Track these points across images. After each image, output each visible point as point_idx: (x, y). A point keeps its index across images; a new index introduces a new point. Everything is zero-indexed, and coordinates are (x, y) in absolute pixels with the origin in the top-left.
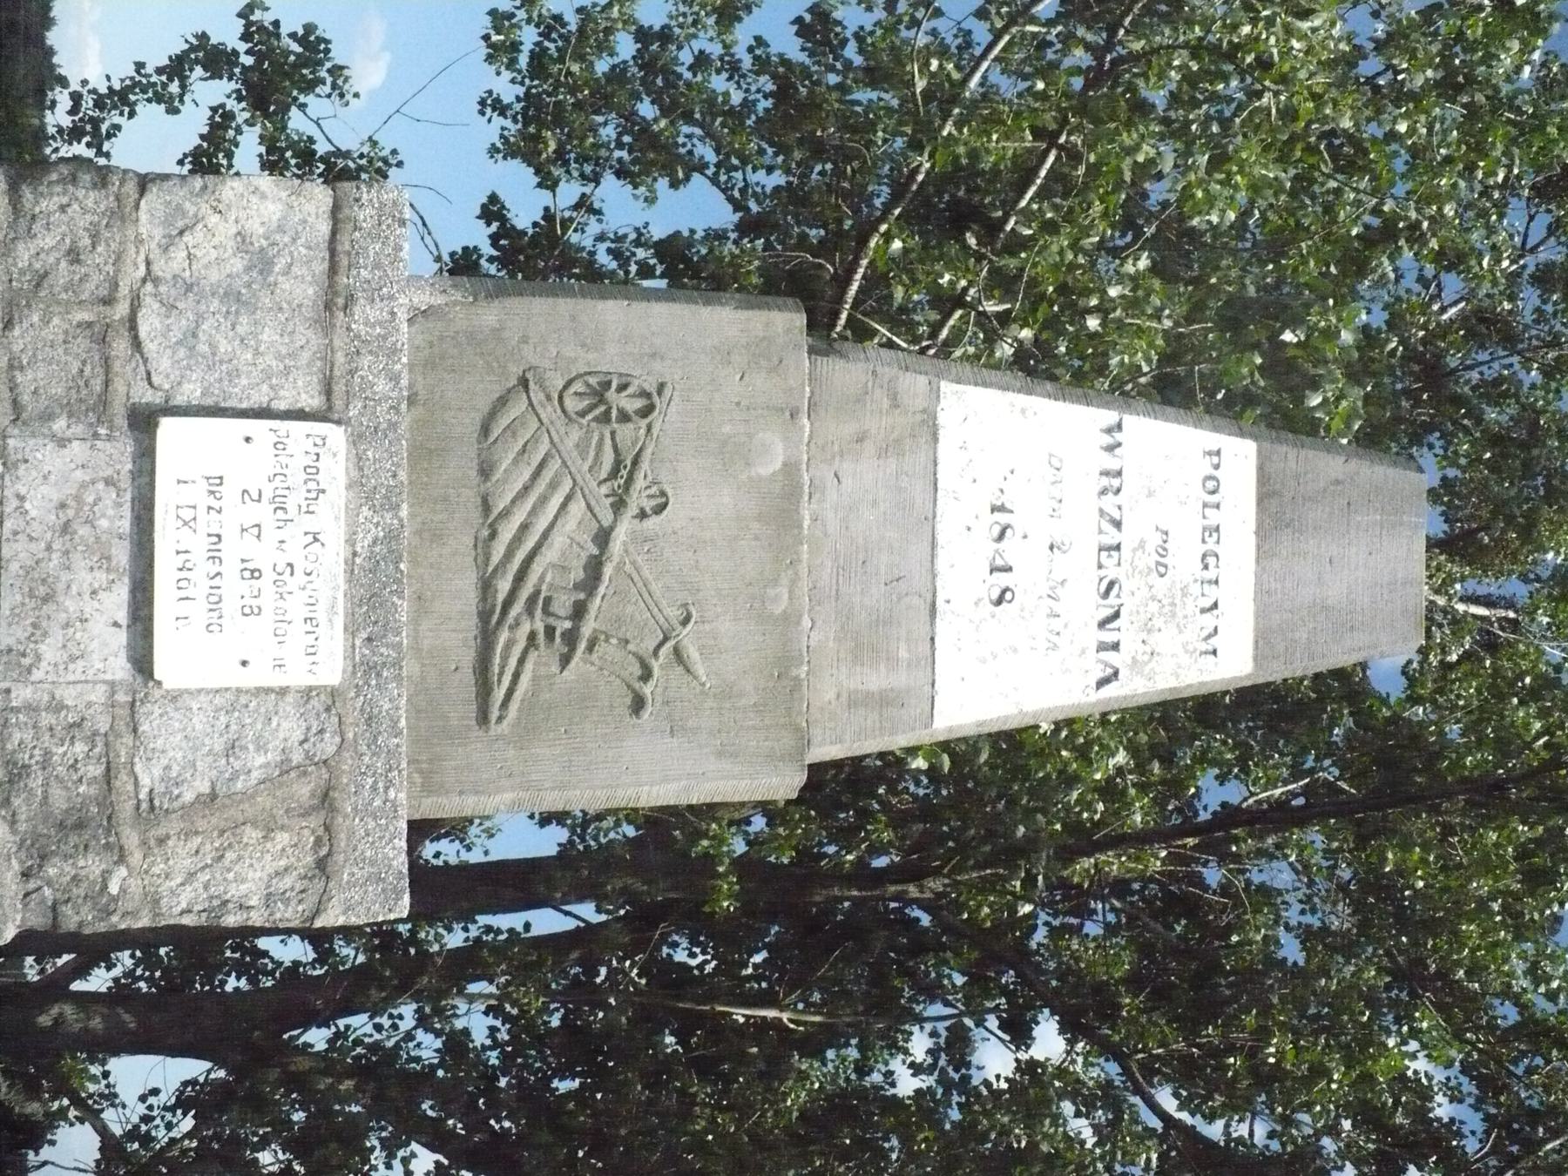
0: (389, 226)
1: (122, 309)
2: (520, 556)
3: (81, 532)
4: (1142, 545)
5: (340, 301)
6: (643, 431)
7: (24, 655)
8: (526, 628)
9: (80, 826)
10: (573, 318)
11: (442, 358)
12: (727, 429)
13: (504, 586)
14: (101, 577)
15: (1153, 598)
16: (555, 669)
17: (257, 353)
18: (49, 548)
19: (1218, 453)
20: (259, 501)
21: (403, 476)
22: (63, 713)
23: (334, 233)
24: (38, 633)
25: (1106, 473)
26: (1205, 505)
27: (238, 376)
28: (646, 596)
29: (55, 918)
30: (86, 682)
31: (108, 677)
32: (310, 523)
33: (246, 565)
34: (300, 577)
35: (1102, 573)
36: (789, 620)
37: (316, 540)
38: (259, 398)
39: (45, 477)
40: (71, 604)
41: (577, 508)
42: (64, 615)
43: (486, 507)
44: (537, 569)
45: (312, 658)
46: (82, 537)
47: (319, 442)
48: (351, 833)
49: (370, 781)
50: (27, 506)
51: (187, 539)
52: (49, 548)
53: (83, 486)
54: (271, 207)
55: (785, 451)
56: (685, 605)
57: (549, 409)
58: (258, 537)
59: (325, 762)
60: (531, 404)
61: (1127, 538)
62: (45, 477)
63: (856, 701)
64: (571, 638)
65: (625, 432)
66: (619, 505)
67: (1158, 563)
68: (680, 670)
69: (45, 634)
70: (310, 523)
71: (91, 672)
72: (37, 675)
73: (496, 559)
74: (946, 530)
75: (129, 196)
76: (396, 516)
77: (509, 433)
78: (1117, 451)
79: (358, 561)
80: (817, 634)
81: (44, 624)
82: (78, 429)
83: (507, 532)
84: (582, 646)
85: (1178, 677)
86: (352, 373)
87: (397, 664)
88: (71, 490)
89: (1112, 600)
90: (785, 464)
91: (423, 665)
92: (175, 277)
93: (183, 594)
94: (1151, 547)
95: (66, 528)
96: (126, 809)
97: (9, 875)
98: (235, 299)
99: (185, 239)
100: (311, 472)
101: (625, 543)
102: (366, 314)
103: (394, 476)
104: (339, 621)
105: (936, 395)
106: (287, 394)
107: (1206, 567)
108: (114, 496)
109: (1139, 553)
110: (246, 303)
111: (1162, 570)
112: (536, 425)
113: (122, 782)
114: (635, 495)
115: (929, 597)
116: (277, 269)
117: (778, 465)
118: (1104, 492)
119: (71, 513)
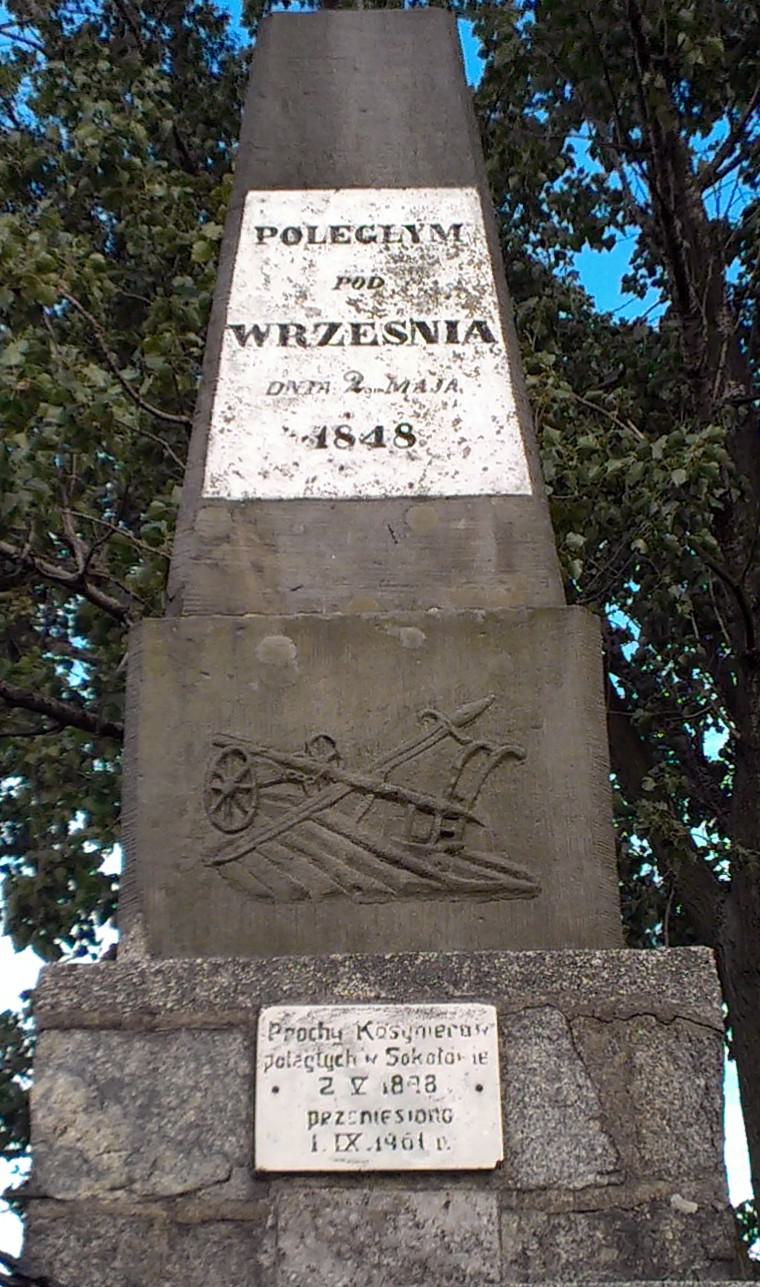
1: (157, 1210)
2: (384, 866)
4: (352, 303)
5: (147, 1018)
6: (259, 760)
9: (633, 1236)
10: (155, 824)
12: (255, 686)
13: (404, 876)
15: (405, 290)
16: (481, 832)
17: (195, 1088)
18: (378, 1266)
19: (260, 230)
20: (331, 1079)
21: (305, 959)
22: (529, 1253)
23: (83, 1027)
25: (284, 341)
26: (312, 241)
27: (217, 1103)
28: (413, 752)
29: (721, 1260)
30: (500, 1231)
31: (495, 1211)
33: (389, 1089)
34: (400, 1042)
35: (380, 340)
36: (430, 626)
37: (365, 1029)
38: (235, 1085)
39: (313, 1270)
40: (430, 1246)
41: (332, 816)
42: (439, 1252)
43: (334, 894)
44: (388, 849)
45: (473, 1030)
47: (276, 1029)
49: (585, 981)
51: (366, 1141)
52: (378, 1266)
55: (273, 633)
56: (420, 720)
57: (241, 842)
59: (568, 1021)
60: (236, 859)
61: (347, 317)
62: (313, 1270)
63: (507, 566)
64: (452, 816)
65: (263, 774)
66: (327, 778)
67: (370, 287)
68: (478, 722)
69: (457, 1268)
73: (379, 884)
74: (345, 488)
76: (342, 963)
78: (263, 329)
79: (383, 995)
80: (445, 603)
81: (446, 1269)
82: (268, 1243)
84: (458, 807)
85: (481, 263)
86: (211, 1005)
87: (478, 960)
89: (407, 331)
90: (286, 633)
93: (417, 1144)
94: (354, 294)
96: (621, 1196)
99: (91, 1157)
100: (304, 1034)
101: (364, 773)
102: (157, 994)
103: (305, 965)
104: (450, 1007)
105: (217, 502)
107: (373, 239)
109: (361, 305)
110: (151, 1099)
111: (377, 281)
112: (254, 854)
113: (592, 1199)
114: (318, 765)
115: (407, 503)
116: (118, 1075)
117: (288, 640)
118: (302, 342)
119: (345, 1247)
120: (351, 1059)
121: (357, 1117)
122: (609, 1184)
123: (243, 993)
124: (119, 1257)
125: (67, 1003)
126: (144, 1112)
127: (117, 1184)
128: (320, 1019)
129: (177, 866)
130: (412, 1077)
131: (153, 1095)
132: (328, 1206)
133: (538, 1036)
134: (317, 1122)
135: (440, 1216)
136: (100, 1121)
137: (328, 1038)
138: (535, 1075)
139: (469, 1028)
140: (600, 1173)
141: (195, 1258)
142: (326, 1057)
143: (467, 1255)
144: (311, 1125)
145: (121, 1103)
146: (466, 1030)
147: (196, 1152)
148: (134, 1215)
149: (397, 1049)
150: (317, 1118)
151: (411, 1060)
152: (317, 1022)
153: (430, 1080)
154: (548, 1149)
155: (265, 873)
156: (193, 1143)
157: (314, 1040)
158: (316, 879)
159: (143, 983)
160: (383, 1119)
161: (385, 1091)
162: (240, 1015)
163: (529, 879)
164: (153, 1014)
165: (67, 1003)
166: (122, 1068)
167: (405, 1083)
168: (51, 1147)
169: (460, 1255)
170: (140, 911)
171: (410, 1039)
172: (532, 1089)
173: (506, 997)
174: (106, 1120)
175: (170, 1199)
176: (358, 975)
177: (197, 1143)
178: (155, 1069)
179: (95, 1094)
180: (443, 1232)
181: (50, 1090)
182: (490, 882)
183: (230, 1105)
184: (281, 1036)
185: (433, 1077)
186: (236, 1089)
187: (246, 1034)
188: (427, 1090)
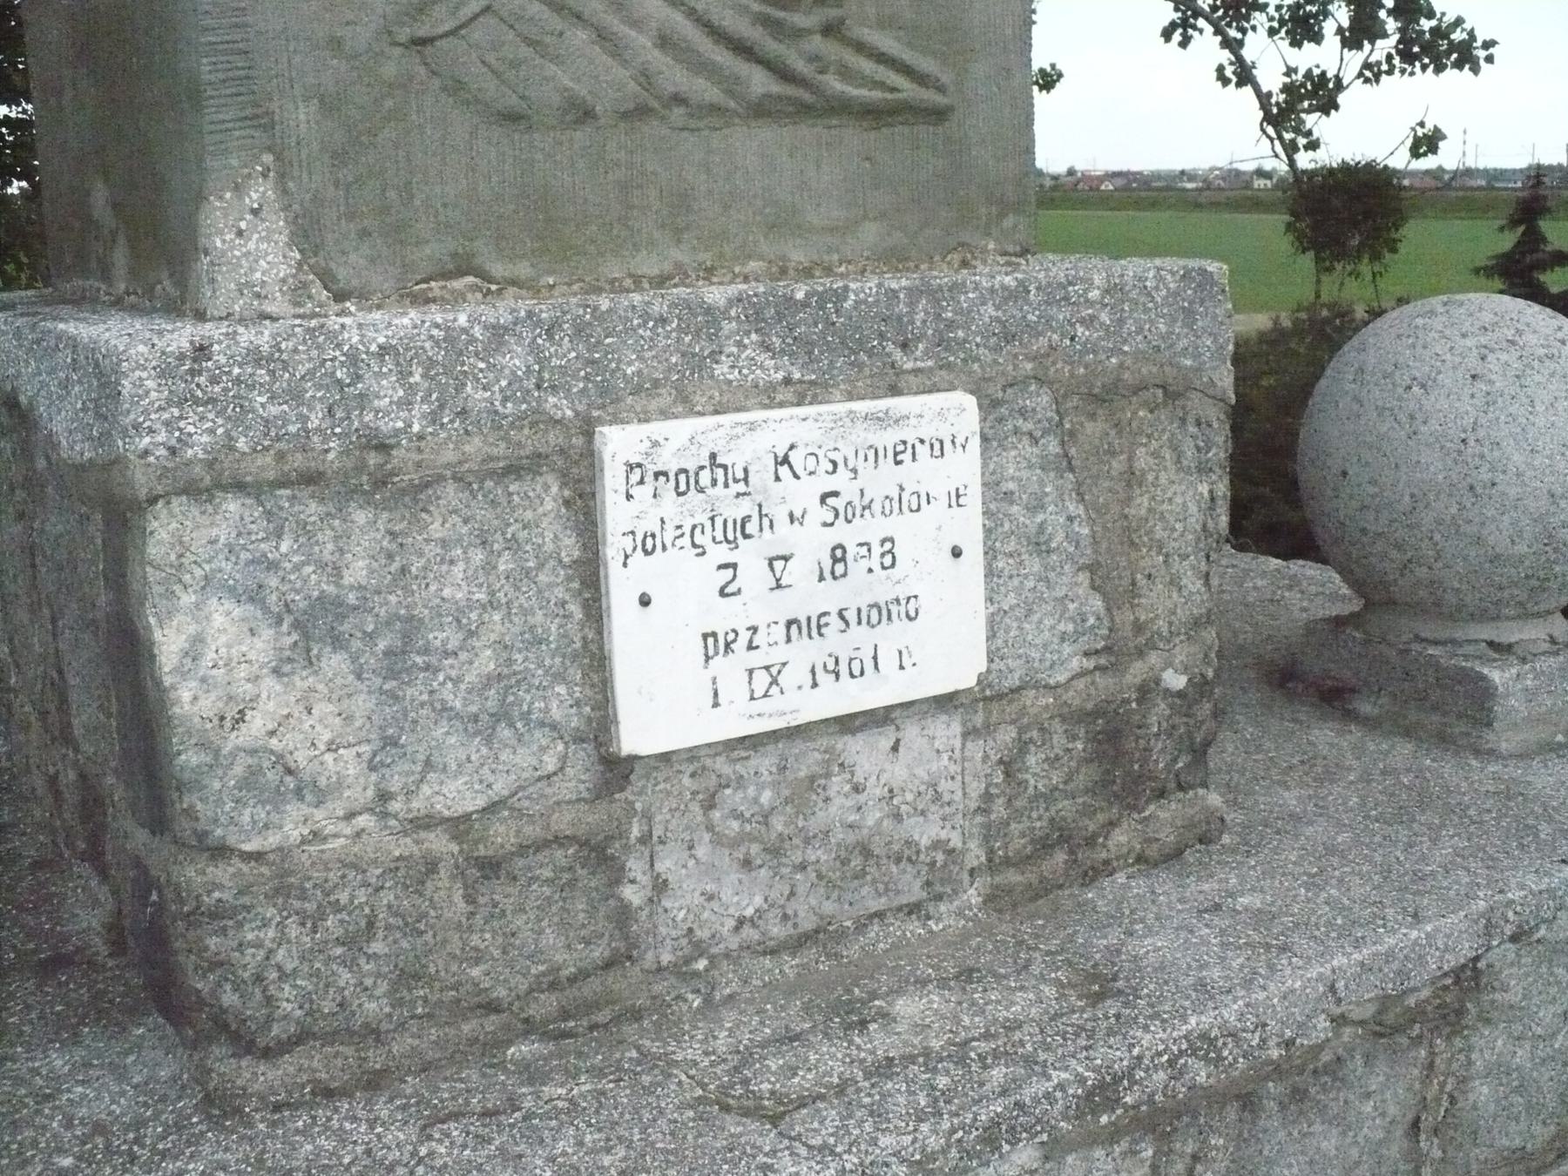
0: (214, 380)
2: (722, 57)
3: (780, 828)
5: (373, 459)
7: (933, 864)
8: (817, 43)
11: (385, 210)
13: (760, 82)
14: (838, 784)
18: (803, 867)
20: (734, 566)
23: (239, 487)
24: (907, 852)
27: (532, 628)
31: (958, 743)
32: (762, 474)
33: (827, 574)
34: (841, 481)
37: (785, 460)
38: (557, 585)
39: (711, 898)
42: (885, 823)
43: (641, 112)
45: (948, 446)
46: (786, 824)
48: (1139, 356)
49: (1080, 330)
50: (749, 912)
51: (794, 676)
52: (803, 867)
53: (718, 840)
54: (218, 620)
58: (786, 559)
60: (453, 32)
62: (711, 898)
70: (762, 474)
71: (954, 768)
72: (956, 841)
73: (705, 90)
75: (239, 873)
77: (510, 75)
79: (797, 376)
81: (896, 847)
82: (636, 866)
83: (675, 77)
88: (724, 859)
91: (865, 217)
92: (372, 768)
95: (775, 851)
97: (1162, 815)
98: (403, 656)
99: (303, 763)
100: (685, 482)
102: (392, 407)
103: (663, 321)
106: (549, 535)
108: (728, 791)
110: (407, 637)
116: (331, 589)
120: (766, 522)
121: (780, 630)
122: (1096, 668)
123: (554, 389)
124: (380, 934)
125: (205, 439)
126: (396, 665)
127: (357, 806)
128: (711, 447)
129: (335, 44)
130: (861, 545)
131: (410, 627)
132: (728, 786)
133: (1016, 431)
134: (717, 653)
135: (888, 766)
136: (312, 690)
137: (726, 485)
138: (1012, 503)
139: (941, 443)
140: (1086, 654)
141: (514, 912)
142: (725, 521)
143: (921, 819)
144: (708, 658)
145: (346, 648)
146: (937, 446)
147: (504, 732)
148: (398, 859)
149: (835, 494)
150: (715, 644)
151: (858, 513)
152: (706, 454)
153: (888, 546)
154: (1027, 626)
155: (515, 64)
156: (495, 719)
157: (701, 491)
158: (610, 83)
159: (359, 377)
160: (819, 627)
161: (821, 578)
162: (554, 438)
163: (941, 89)
164: (383, 448)
165: (205, 439)
166: (337, 573)
167: (850, 557)
168: (217, 753)
169: (913, 820)
170: (269, 149)
171: (855, 471)
172: (1007, 526)
173: (976, 366)
174: (320, 687)
175: (459, 826)
176: (754, 337)
177: (502, 715)
178: (404, 570)
179: (295, 637)
180: (891, 791)
181: (198, 640)
182: (889, 96)
183: (553, 628)
184: (648, 489)
185: (892, 540)
186: (560, 592)
187: (565, 478)
188: (884, 568)
